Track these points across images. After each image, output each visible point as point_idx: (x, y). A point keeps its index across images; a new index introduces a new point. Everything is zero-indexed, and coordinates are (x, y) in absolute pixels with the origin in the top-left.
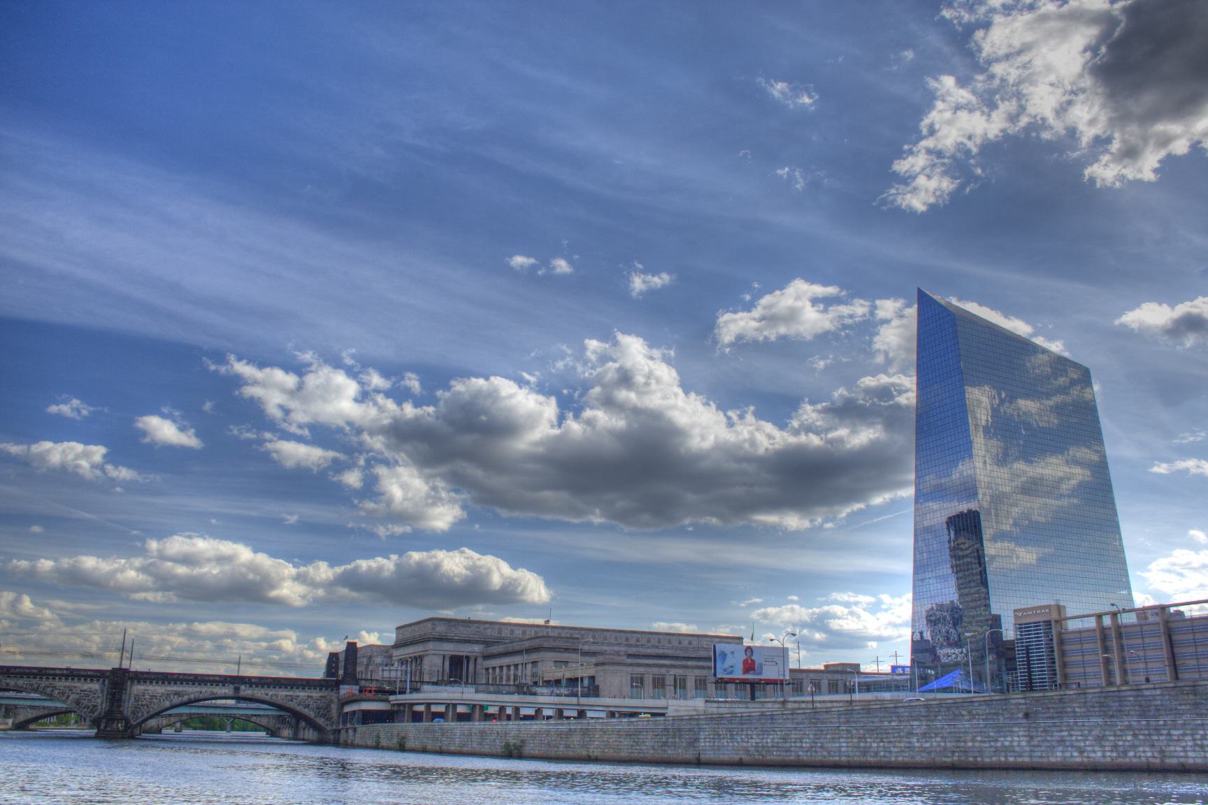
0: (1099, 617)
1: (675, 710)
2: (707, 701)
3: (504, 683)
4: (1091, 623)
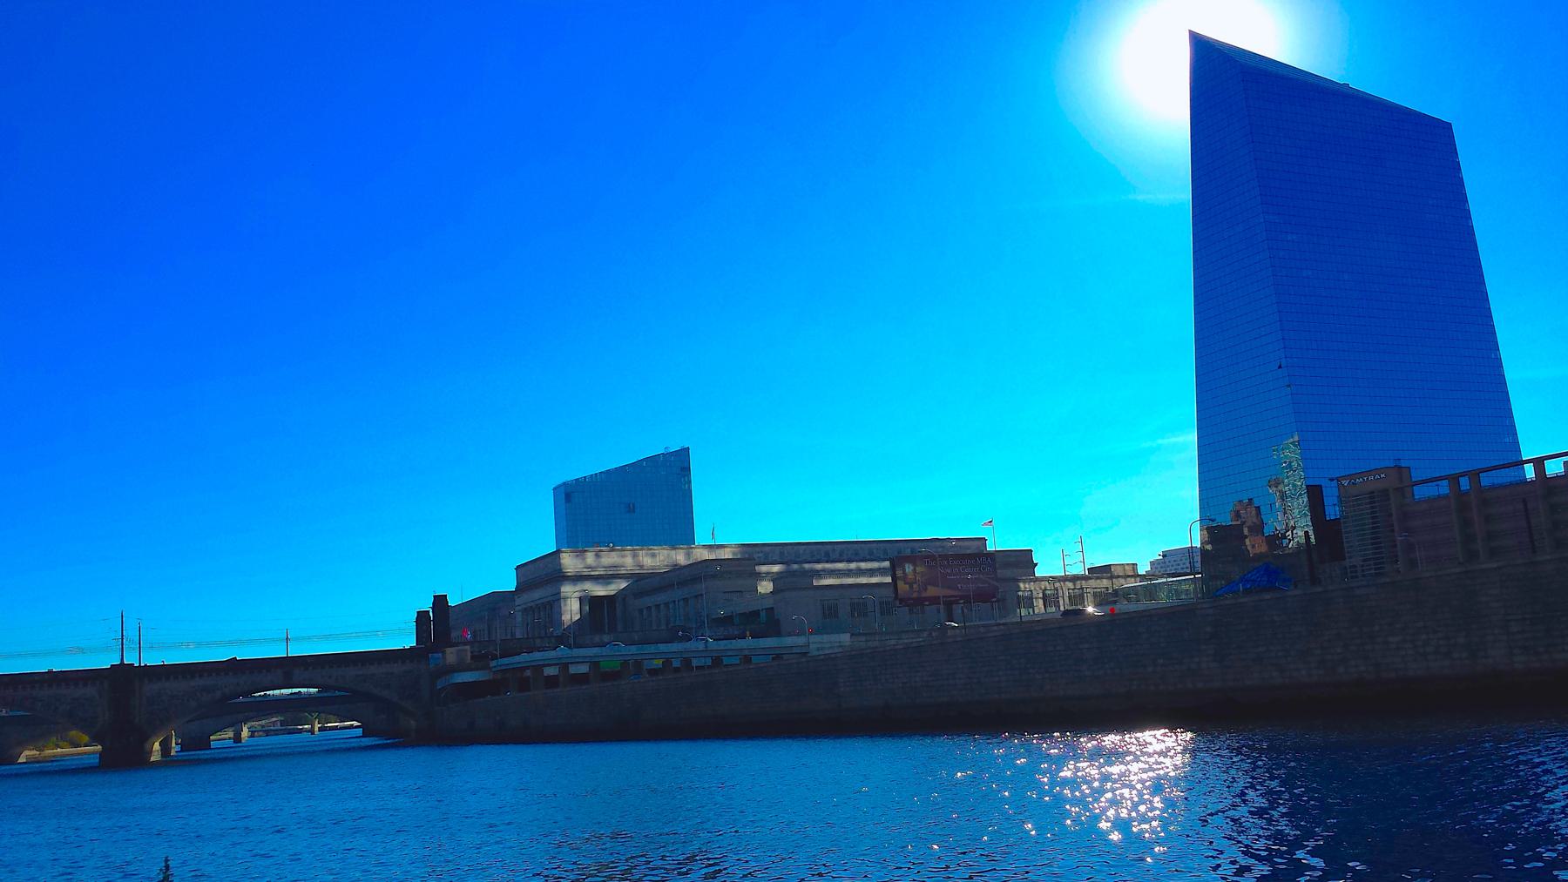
0: (1454, 479)
1: (818, 649)
2: (852, 635)
3: (655, 628)
4: (1444, 488)
